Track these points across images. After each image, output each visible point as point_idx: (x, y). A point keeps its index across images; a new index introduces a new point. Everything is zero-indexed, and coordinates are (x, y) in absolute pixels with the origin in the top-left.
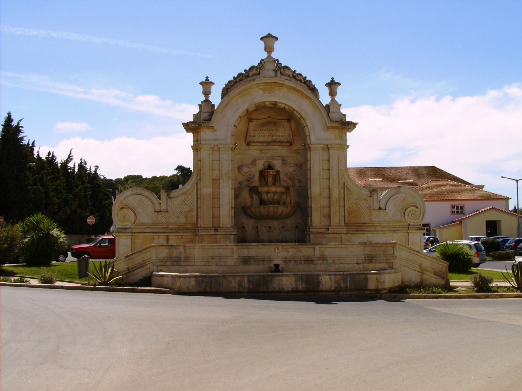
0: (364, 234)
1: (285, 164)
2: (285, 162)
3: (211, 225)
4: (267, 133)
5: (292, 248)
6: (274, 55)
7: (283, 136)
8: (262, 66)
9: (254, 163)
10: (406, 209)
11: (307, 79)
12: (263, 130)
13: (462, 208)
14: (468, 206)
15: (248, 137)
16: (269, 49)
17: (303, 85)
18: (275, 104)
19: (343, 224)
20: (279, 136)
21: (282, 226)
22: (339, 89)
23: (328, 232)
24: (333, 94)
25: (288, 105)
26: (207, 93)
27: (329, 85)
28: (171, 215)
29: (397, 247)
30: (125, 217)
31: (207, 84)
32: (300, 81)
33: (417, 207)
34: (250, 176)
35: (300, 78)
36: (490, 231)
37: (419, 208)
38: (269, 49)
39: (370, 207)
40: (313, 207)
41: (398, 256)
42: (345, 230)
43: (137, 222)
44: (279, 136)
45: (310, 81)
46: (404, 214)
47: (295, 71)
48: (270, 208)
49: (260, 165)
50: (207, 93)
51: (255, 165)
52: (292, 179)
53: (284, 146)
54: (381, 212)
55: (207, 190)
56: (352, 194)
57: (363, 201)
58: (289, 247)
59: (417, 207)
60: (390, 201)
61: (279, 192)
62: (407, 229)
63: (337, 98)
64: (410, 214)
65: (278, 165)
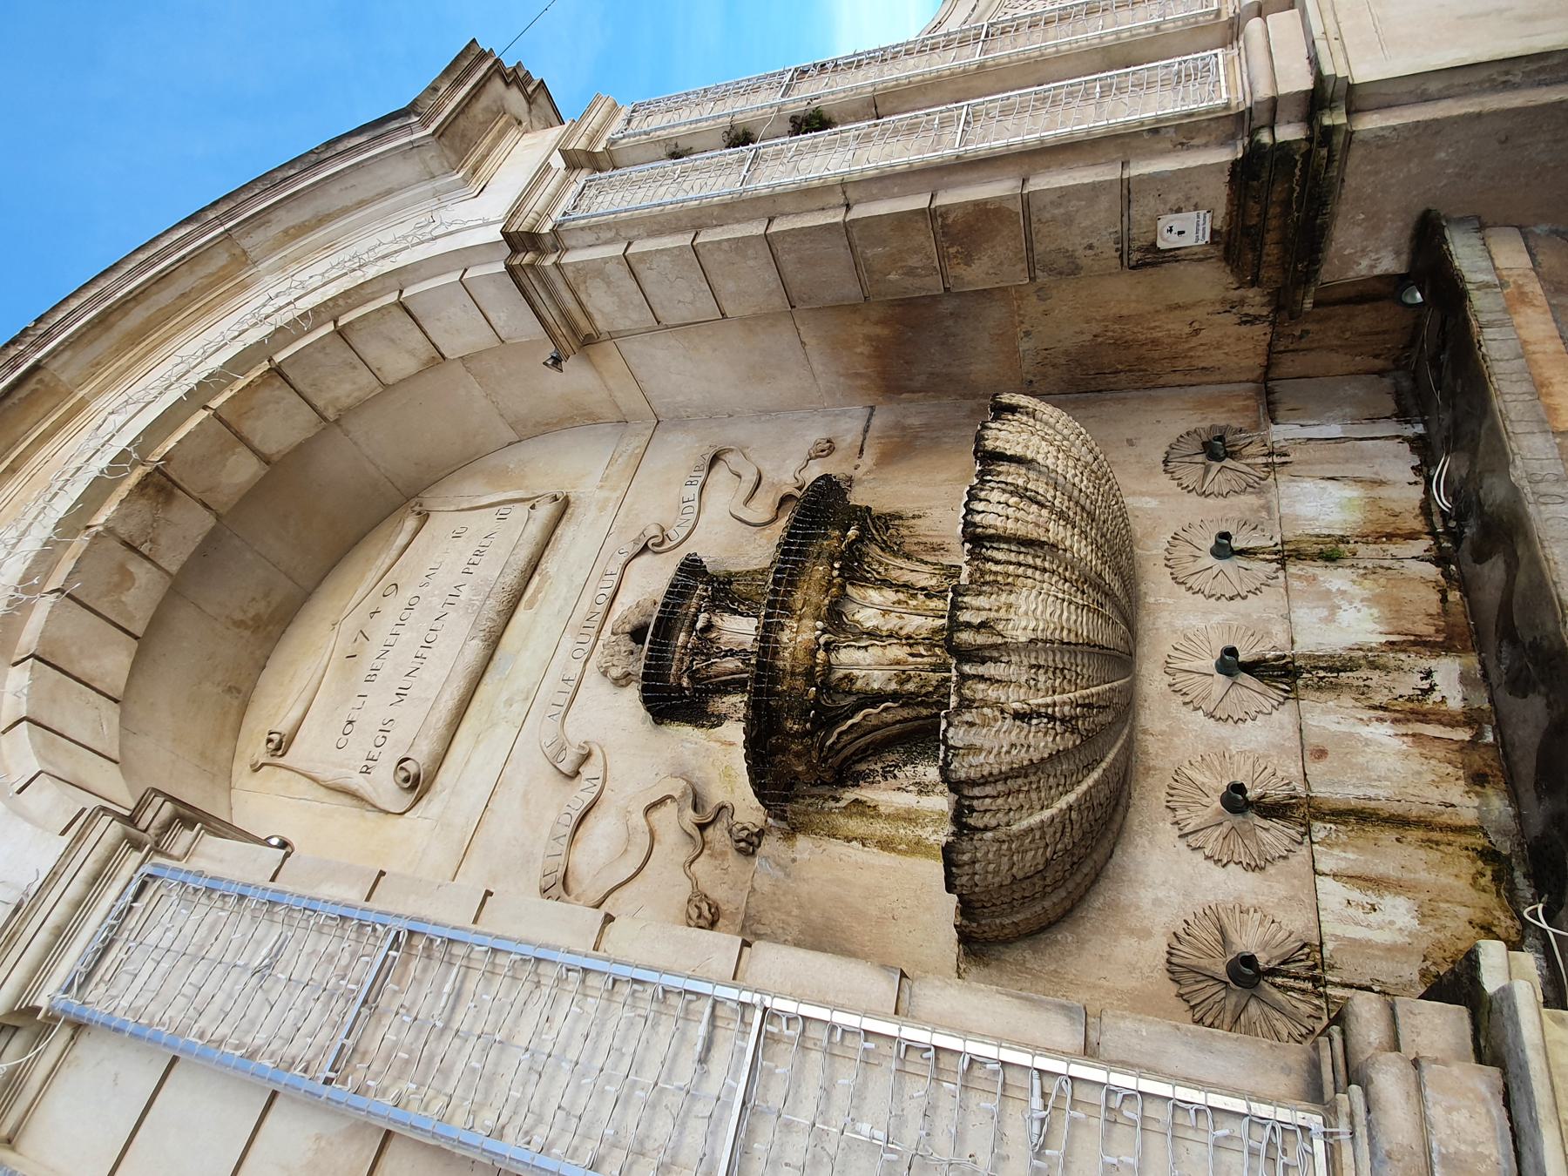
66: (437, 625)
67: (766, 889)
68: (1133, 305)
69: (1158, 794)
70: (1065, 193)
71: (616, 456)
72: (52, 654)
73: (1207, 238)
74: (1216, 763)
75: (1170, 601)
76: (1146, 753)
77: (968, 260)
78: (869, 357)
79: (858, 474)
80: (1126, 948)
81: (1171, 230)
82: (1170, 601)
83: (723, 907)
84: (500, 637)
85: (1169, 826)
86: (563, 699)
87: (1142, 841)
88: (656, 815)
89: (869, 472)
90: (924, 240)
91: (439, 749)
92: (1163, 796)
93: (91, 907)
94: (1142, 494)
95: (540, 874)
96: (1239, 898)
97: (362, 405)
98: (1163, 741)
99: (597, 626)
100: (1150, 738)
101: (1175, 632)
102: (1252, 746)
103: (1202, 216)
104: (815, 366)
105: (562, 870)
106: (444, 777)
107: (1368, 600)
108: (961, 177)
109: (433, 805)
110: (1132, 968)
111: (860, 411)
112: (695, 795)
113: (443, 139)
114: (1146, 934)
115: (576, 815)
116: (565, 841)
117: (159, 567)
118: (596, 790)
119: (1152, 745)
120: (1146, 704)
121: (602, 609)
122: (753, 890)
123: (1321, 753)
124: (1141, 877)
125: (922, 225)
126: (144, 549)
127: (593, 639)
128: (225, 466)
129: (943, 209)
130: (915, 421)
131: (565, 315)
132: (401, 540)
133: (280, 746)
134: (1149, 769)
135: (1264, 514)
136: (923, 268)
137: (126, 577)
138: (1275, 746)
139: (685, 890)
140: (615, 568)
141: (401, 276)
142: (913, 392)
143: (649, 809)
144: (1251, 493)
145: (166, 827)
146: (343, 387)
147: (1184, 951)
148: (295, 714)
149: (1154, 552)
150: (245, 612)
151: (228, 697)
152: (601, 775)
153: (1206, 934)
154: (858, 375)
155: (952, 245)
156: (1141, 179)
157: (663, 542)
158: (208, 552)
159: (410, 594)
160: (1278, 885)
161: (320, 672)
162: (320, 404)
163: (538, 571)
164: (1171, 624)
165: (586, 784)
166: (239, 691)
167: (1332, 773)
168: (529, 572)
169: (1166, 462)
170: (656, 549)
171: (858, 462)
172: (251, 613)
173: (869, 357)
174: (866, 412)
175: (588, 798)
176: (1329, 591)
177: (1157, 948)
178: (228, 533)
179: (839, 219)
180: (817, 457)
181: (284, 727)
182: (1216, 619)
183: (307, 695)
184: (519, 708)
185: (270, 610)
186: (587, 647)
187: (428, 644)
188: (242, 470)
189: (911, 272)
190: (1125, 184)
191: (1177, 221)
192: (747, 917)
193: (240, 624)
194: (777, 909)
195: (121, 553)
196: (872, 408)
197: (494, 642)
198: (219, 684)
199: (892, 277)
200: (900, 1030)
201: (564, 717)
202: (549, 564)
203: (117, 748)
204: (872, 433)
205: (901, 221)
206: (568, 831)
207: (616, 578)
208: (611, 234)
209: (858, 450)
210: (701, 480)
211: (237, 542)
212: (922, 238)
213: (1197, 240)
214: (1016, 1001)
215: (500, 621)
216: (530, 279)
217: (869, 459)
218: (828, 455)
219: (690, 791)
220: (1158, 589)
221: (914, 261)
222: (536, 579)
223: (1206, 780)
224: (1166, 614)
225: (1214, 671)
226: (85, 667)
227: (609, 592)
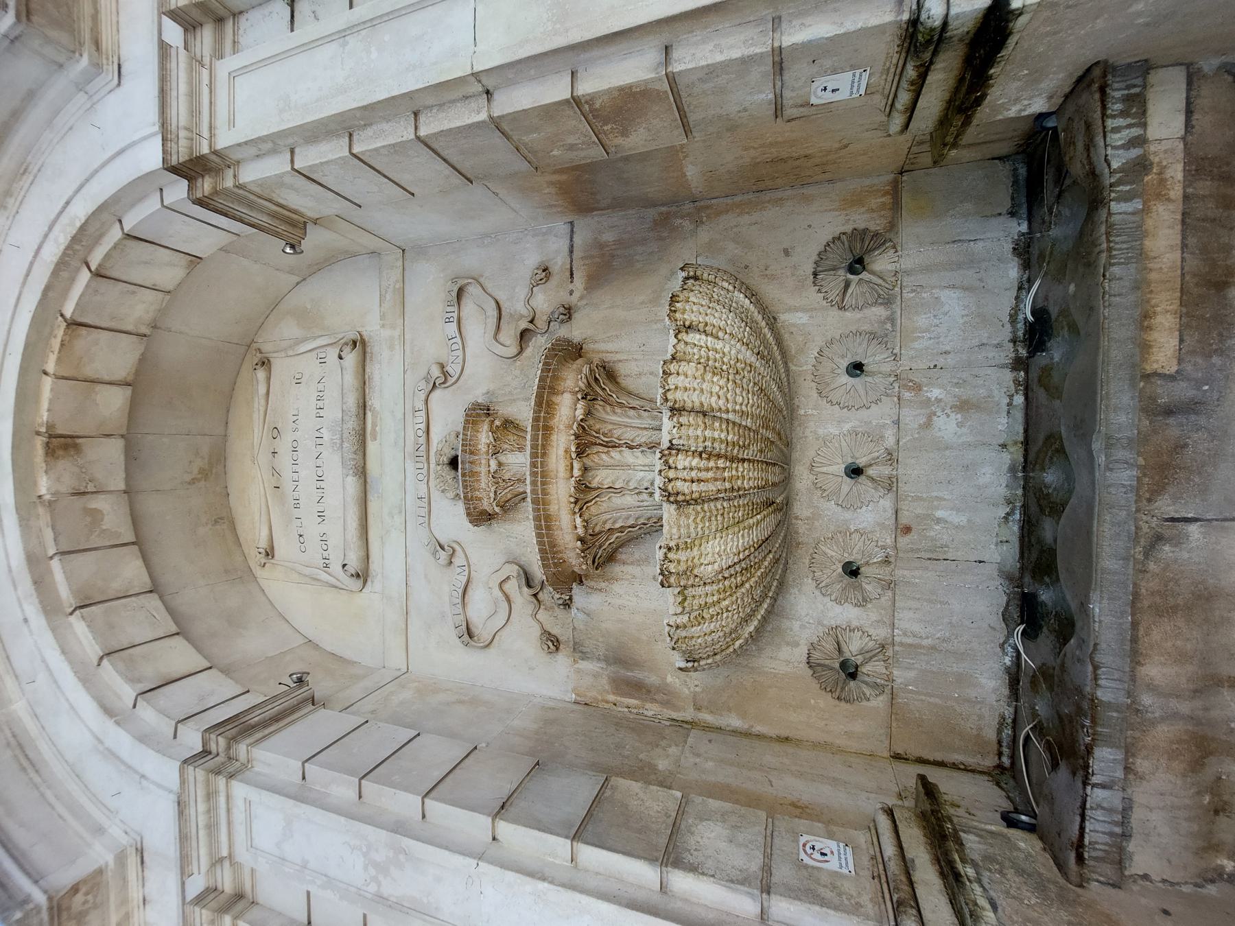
4: (306, 473)
7: (321, 387)
12: (296, 495)
15: (324, 576)
20: (322, 413)
21: (845, 379)
44: (322, 413)
48: (680, 485)
52: (524, 324)
61: (581, 405)
66: (319, 462)
67: (582, 627)
68: (786, 134)
69: (804, 560)
70: (711, 71)
71: (383, 292)
72: (86, 598)
73: (862, 92)
74: (841, 540)
75: (815, 412)
76: (797, 533)
77: (625, 133)
78: (557, 194)
79: (574, 299)
80: (785, 653)
81: (825, 89)
82: (815, 412)
83: (561, 639)
84: (364, 467)
85: (810, 581)
86: (424, 512)
87: (795, 591)
88: (506, 587)
89: (581, 298)
90: (577, 129)
91: (363, 553)
92: (807, 561)
93: (216, 808)
94: (796, 309)
95: (454, 628)
96: (850, 622)
97: (163, 311)
98: (808, 524)
99: (423, 454)
100: (800, 522)
101: (817, 439)
102: (865, 524)
103: (857, 75)
104: (512, 205)
105: (464, 624)
106: (374, 566)
107: (956, 406)
108: (596, 53)
109: (375, 585)
110: (788, 662)
111: (561, 227)
112: (526, 573)
113: (34, 18)
114: (797, 645)
115: (460, 591)
116: (460, 606)
117: (111, 492)
118: (466, 573)
119: (801, 527)
120: (798, 498)
121: (422, 440)
122: (574, 629)
123: (907, 530)
124: (793, 612)
125: (569, 112)
126: (91, 488)
127: (426, 465)
128: (97, 405)
129: (588, 98)
130: (609, 237)
131: (274, 215)
132: (262, 390)
133: (269, 553)
134: (799, 544)
135: (889, 326)
136: (583, 143)
137: (95, 516)
138: (879, 524)
139: (537, 631)
140: (420, 405)
141: (109, 210)
142: (602, 210)
143: (501, 584)
144: (881, 304)
145: (229, 748)
146: (139, 309)
147: (816, 655)
148: (265, 533)
149: (805, 368)
150: (191, 473)
151: (218, 527)
152: (465, 563)
153: (830, 646)
154: (551, 206)
155: (606, 124)
156: (794, 47)
157: (446, 379)
158: (132, 455)
159: (290, 439)
160: (871, 614)
161: (263, 500)
162: (130, 328)
163: (368, 408)
164: (815, 432)
165: (459, 570)
166: (221, 518)
167: (912, 543)
168: (361, 412)
169: (815, 274)
170: (443, 386)
171: (571, 287)
172: (196, 471)
173: (557, 194)
174: (567, 228)
175: (464, 580)
176: (929, 399)
177: (801, 653)
178: (139, 436)
179: (483, 116)
180: (538, 285)
181: (263, 544)
182: (847, 427)
183: (264, 518)
184: (398, 520)
185: (206, 461)
186: (424, 471)
187: (320, 479)
188: (113, 402)
189: (572, 147)
190: (777, 52)
191: (831, 82)
192: (575, 643)
193: (193, 481)
194: (590, 638)
195: (79, 502)
196: (571, 223)
197: (362, 473)
198: (207, 524)
199: (555, 153)
200: (663, 888)
201: (429, 524)
202: (374, 402)
203: (172, 623)
204: (577, 254)
205: (549, 112)
206: (459, 601)
207: (423, 413)
208: (269, 145)
209: (568, 274)
210: (455, 315)
211: (150, 437)
212: (574, 122)
213: (852, 93)
214: (724, 888)
215: (359, 457)
216: (221, 201)
217: (579, 283)
218: (546, 282)
219: (521, 572)
220: (809, 403)
221: (571, 140)
222: (369, 414)
223: (834, 554)
224: (812, 423)
225: (843, 474)
226: (116, 586)
227: (423, 426)
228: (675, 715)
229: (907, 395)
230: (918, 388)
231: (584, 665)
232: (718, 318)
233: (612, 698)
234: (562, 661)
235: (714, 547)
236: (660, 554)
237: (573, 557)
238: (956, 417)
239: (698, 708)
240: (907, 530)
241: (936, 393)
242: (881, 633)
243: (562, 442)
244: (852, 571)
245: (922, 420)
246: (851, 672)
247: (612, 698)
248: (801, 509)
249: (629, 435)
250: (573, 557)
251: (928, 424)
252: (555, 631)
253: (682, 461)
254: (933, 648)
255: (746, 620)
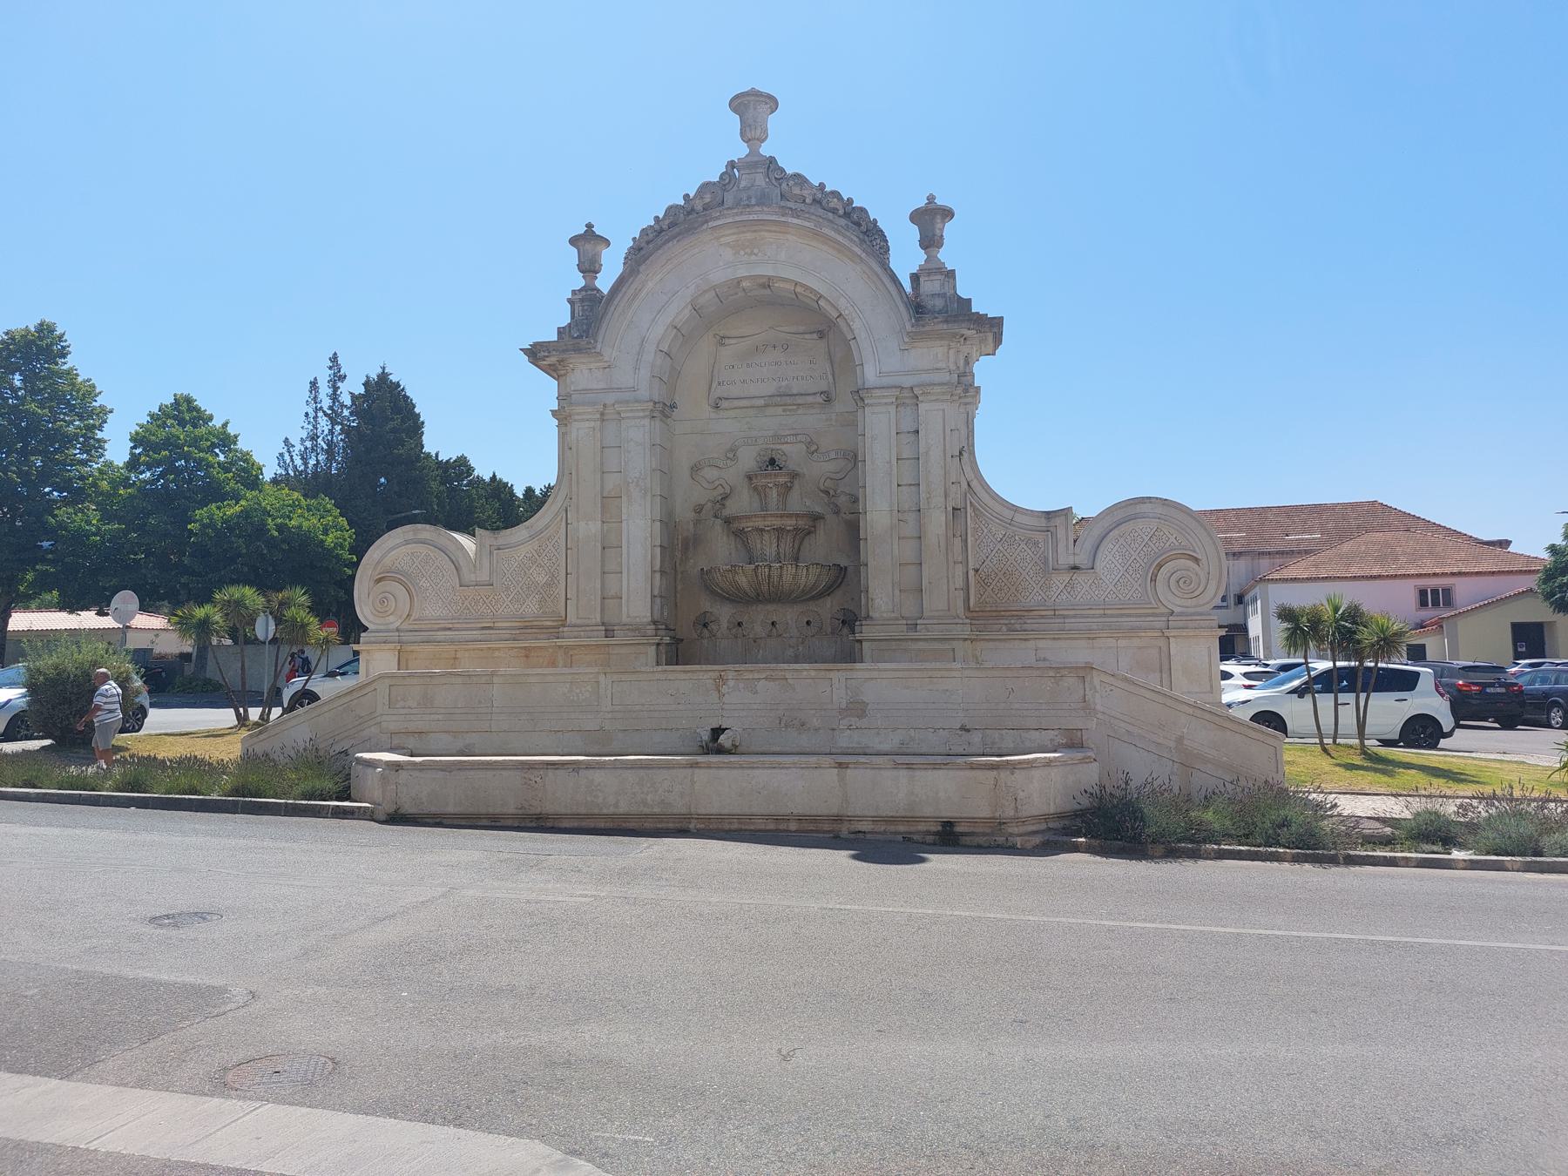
0: (1025, 640)
1: (813, 453)
2: (813, 449)
3: (599, 620)
5: (766, 678)
6: (766, 150)
8: (730, 181)
9: (732, 453)
10: (1160, 566)
11: (828, 189)
13: (1447, 592)
14: (1464, 591)
15: (714, 385)
16: (752, 132)
17: (843, 222)
18: (767, 283)
19: (961, 611)
21: (806, 620)
22: (950, 230)
23: (912, 635)
24: (930, 241)
25: (803, 285)
26: (589, 268)
27: (917, 217)
28: (502, 594)
29: (1097, 679)
30: (384, 602)
31: (588, 242)
32: (834, 211)
33: (1196, 560)
34: (722, 491)
35: (834, 203)
36: (1524, 649)
37: (1204, 561)
38: (752, 132)
39: (1046, 562)
40: (871, 563)
41: (1099, 707)
42: (966, 631)
43: (415, 615)
45: (862, 210)
46: (1153, 580)
47: (850, 201)
49: (748, 459)
50: (589, 268)
51: (735, 458)
52: (832, 492)
53: (811, 405)
54: (1080, 578)
55: (589, 528)
56: (990, 526)
57: (1023, 545)
58: (756, 676)
59: (1196, 560)
60: (1107, 546)
62: (1163, 625)
63: (946, 255)
64: (1173, 581)
65: (793, 453)
153: (713, 619)
169: (844, 609)
182: (790, 621)
192: (700, 520)
228: (677, 564)
229: (800, 639)
230: (803, 643)
231: (691, 524)
232: (812, 579)
233: (680, 537)
234: (691, 515)
235: (744, 579)
236: (741, 564)
237: (735, 525)
238: (793, 655)
239: (682, 573)
240: (755, 642)
241: (801, 649)
242: (719, 634)
243: (777, 523)
244: (740, 624)
245: (792, 645)
246: (705, 625)
247: (680, 537)
248: (760, 607)
249: (782, 546)
250: (735, 525)
251: (790, 646)
252: (704, 512)
253: (767, 570)
254: (716, 651)
255: (721, 589)
